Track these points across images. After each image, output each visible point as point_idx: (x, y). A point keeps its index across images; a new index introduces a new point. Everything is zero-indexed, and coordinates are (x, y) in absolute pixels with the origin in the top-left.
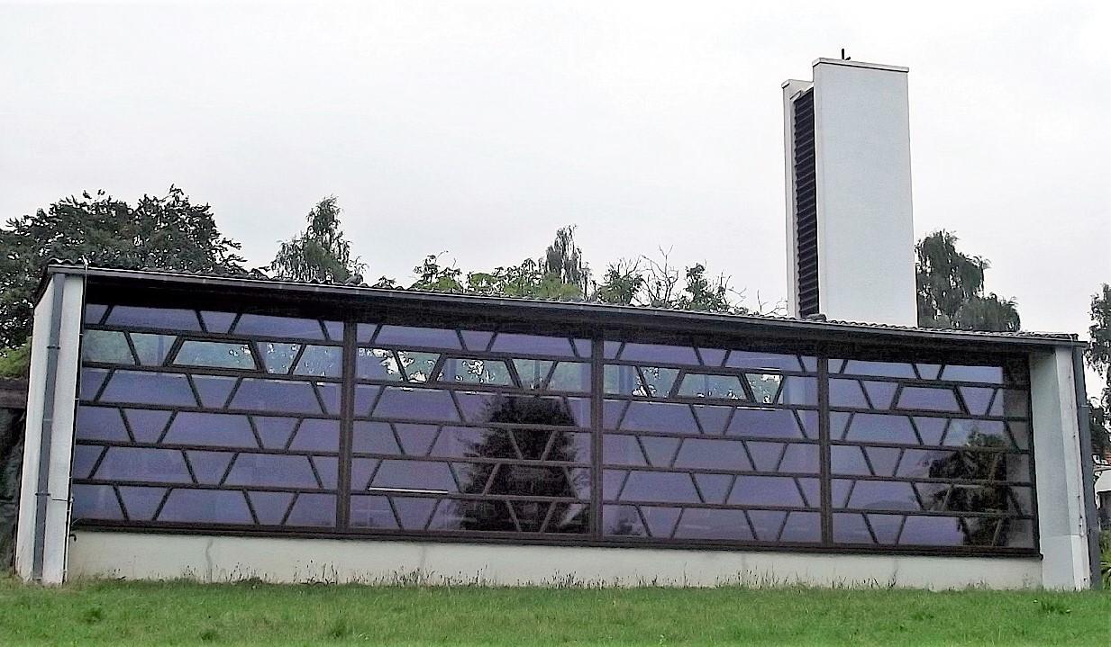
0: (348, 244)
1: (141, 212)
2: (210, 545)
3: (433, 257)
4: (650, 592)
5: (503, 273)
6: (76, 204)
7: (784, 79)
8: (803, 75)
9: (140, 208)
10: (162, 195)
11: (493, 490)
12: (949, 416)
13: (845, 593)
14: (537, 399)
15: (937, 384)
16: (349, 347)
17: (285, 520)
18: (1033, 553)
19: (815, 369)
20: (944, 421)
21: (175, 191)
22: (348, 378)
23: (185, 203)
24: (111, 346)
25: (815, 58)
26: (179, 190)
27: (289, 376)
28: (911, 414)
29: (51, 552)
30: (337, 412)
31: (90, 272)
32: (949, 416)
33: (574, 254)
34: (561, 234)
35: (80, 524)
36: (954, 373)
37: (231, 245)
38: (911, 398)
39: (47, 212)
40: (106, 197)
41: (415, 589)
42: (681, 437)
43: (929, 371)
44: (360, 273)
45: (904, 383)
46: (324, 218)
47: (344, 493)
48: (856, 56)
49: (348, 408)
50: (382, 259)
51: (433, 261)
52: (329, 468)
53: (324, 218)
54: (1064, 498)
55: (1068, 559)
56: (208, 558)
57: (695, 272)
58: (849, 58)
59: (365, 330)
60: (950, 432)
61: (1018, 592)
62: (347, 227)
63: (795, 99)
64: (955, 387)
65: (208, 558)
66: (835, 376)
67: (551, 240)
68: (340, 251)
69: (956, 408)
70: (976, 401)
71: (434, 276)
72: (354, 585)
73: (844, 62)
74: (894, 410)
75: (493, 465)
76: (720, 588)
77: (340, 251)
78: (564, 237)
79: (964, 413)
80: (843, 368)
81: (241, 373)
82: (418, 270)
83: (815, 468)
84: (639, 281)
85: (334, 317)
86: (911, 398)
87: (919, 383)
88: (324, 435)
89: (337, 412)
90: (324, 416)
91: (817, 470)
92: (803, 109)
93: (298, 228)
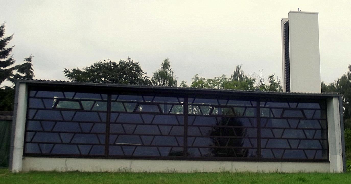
0: (173, 72)
1: (120, 65)
2: (66, 160)
3: (197, 75)
4: (196, 174)
5: (217, 79)
6: (102, 63)
7: (281, 18)
8: (286, 16)
9: (120, 63)
10: (126, 60)
11: (228, 146)
12: (300, 119)
13: (265, 174)
14: (237, 118)
15: (296, 109)
16: (109, 102)
17: (133, 154)
18: (327, 161)
19: (256, 106)
20: (298, 120)
21: (129, 58)
22: (109, 112)
23: (132, 62)
24: (35, 103)
25: (289, 11)
26: (130, 58)
27: (91, 111)
28: (287, 118)
29: (17, 163)
30: (183, 124)
31: (27, 82)
32: (300, 119)
33: (241, 73)
34: (238, 67)
35: (26, 155)
36: (301, 105)
37: (144, 73)
38: (287, 114)
39: (93, 65)
40: (109, 61)
41: (120, 173)
42: (246, 128)
43: (293, 105)
44: (176, 80)
45: (284, 109)
46: (166, 65)
47: (186, 147)
48: (302, 10)
49: (259, 122)
50: (183, 78)
51: (197, 76)
52: (181, 140)
53: (166, 65)
54: (335, 143)
55: (337, 163)
56: (66, 164)
57: (272, 77)
58: (300, 11)
59: (114, 97)
60: (300, 124)
61: (255, 173)
62: (172, 66)
63: (284, 24)
64: (302, 110)
65: (66, 164)
66: (263, 107)
67: (235, 69)
68: (171, 74)
69: (302, 116)
70: (309, 114)
71: (198, 80)
72: (107, 172)
73: (299, 12)
74: (282, 117)
75: (228, 138)
76: (204, 173)
77: (171, 74)
78: (238, 68)
79: (305, 118)
80: (265, 105)
81: (76, 110)
82: (193, 78)
83: (104, 131)
84: (254, 80)
85: (105, 93)
86: (287, 114)
87: (290, 109)
88: (101, 128)
89: (183, 124)
90: (101, 122)
91: (256, 136)
92: (286, 27)
93: (158, 68)
